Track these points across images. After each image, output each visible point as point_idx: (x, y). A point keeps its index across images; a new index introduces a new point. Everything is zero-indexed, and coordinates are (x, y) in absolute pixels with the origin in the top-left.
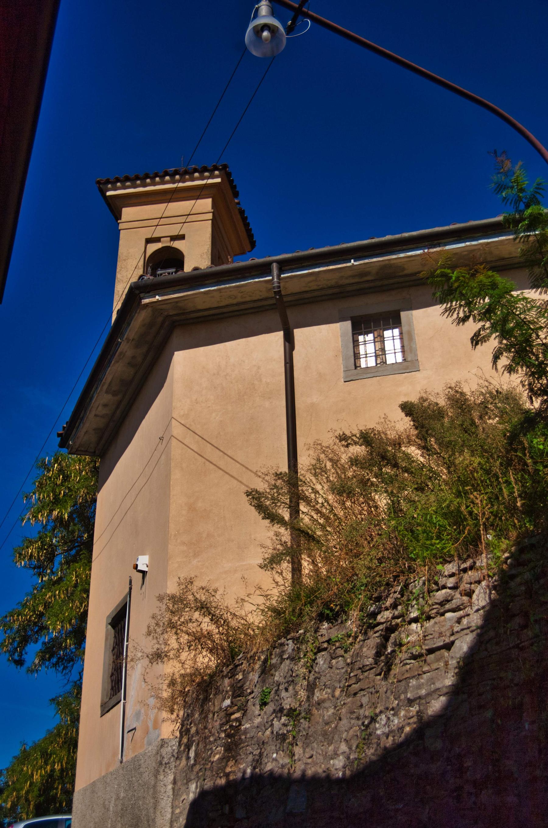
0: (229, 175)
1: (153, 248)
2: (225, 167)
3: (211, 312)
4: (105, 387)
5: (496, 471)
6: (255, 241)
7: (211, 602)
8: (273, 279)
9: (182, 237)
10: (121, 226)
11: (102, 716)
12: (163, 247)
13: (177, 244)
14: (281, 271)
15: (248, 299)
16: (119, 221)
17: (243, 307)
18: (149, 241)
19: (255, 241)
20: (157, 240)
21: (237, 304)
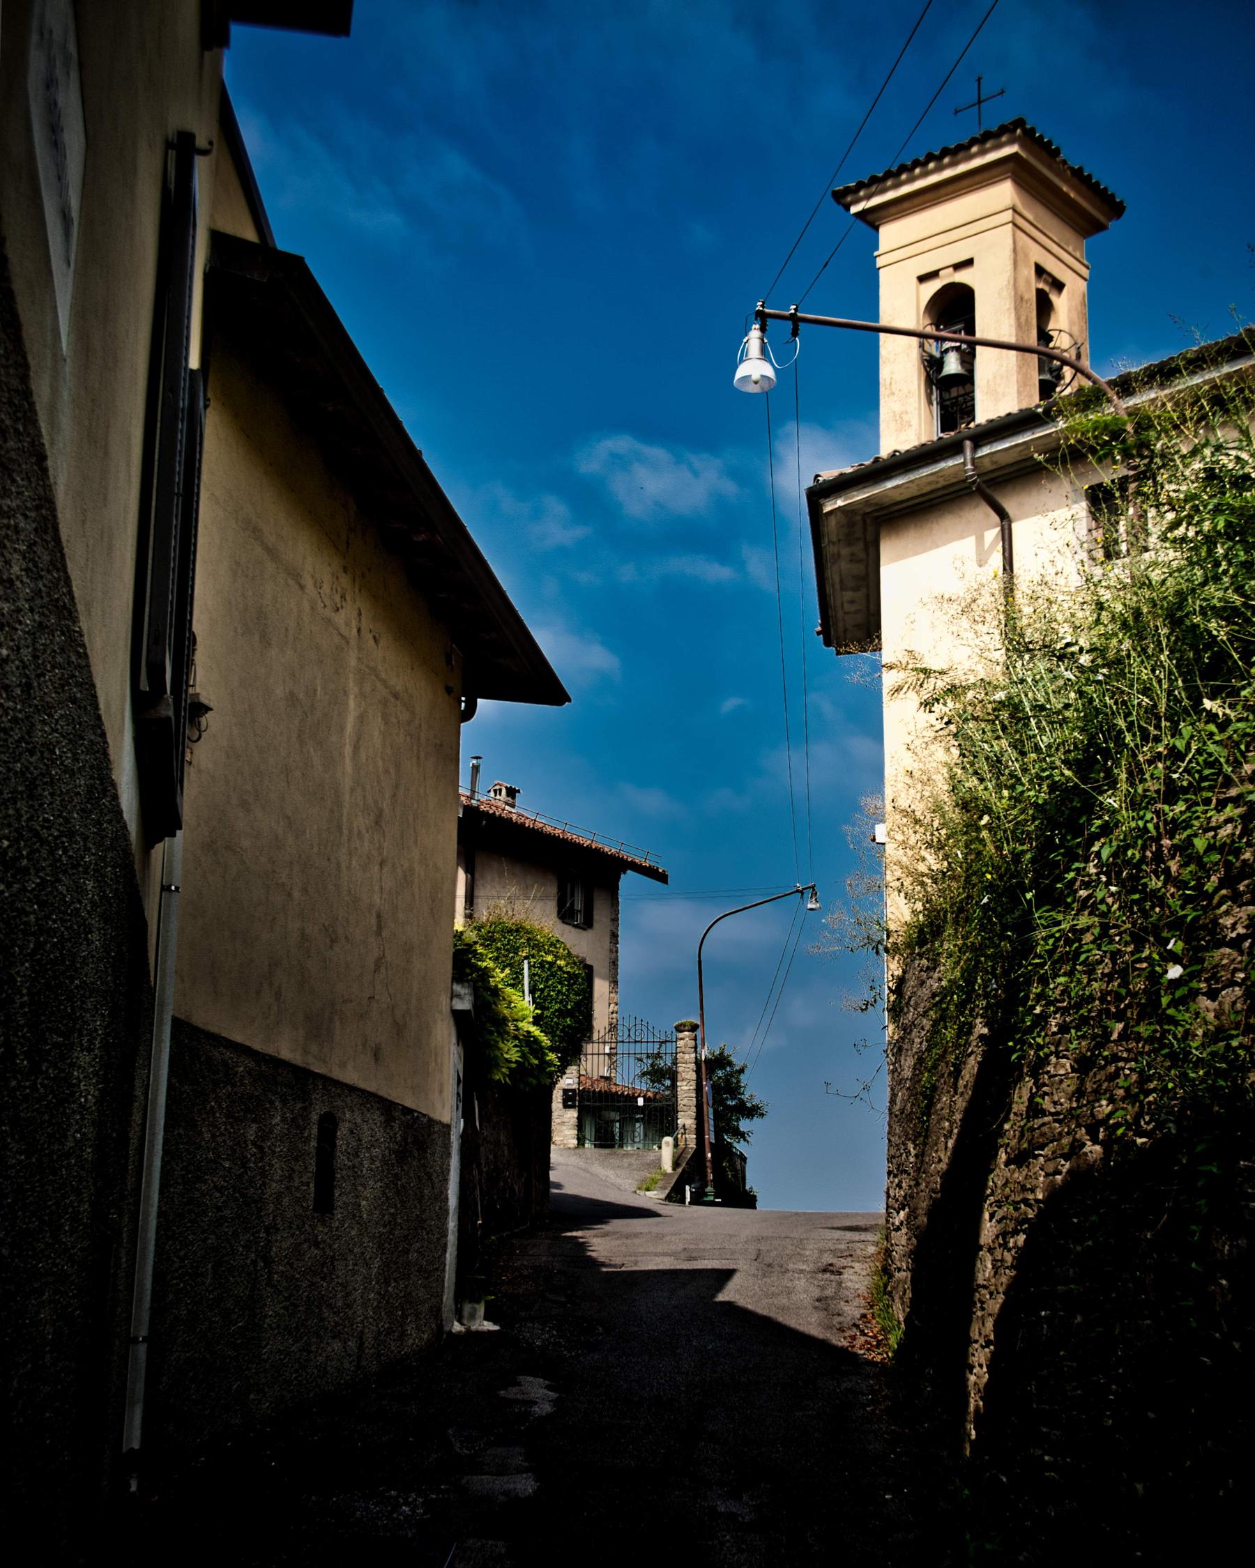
0: (1029, 133)
1: (934, 286)
2: (1020, 123)
3: (917, 501)
4: (837, 586)
5: (1224, 714)
6: (1121, 202)
7: (918, 878)
8: (964, 464)
9: (969, 263)
10: (880, 262)
11: (211, 709)
12: (944, 287)
13: (962, 277)
14: (976, 447)
15: (954, 480)
16: (876, 254)
17: (952, 489)
18: (922, 279)
19: (1121, 202)
20: (934, 275)
21: (944, 487)
